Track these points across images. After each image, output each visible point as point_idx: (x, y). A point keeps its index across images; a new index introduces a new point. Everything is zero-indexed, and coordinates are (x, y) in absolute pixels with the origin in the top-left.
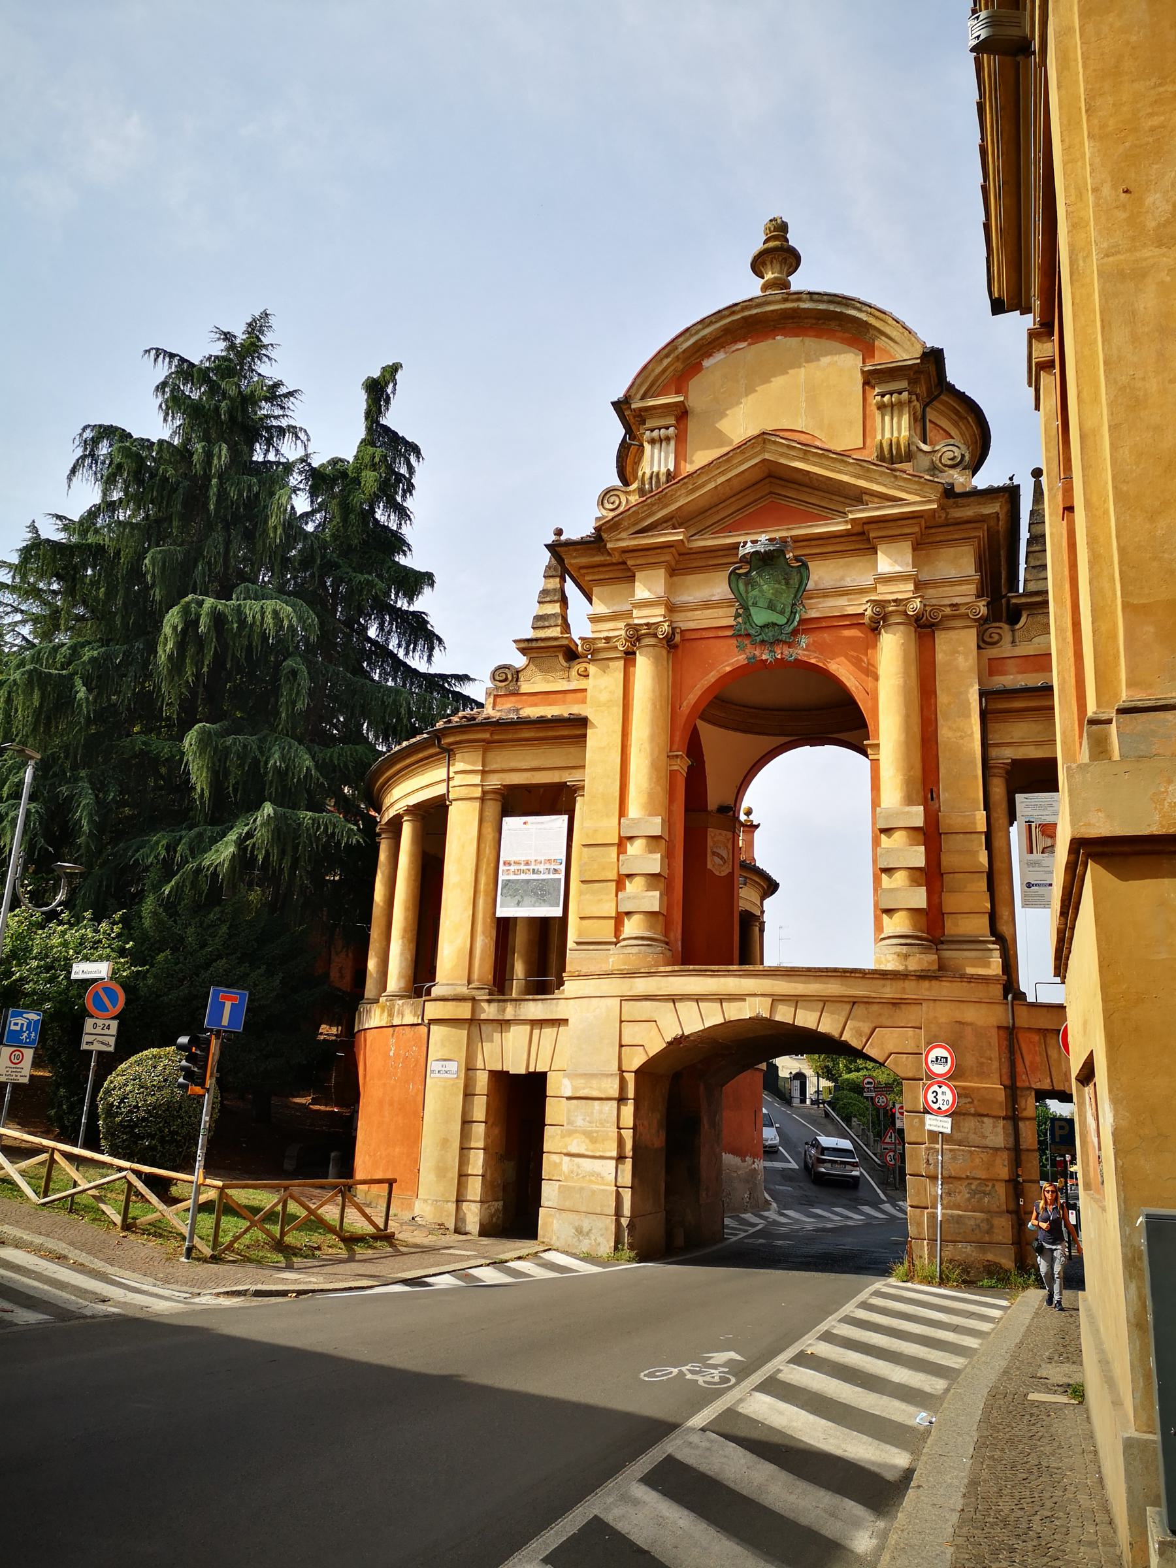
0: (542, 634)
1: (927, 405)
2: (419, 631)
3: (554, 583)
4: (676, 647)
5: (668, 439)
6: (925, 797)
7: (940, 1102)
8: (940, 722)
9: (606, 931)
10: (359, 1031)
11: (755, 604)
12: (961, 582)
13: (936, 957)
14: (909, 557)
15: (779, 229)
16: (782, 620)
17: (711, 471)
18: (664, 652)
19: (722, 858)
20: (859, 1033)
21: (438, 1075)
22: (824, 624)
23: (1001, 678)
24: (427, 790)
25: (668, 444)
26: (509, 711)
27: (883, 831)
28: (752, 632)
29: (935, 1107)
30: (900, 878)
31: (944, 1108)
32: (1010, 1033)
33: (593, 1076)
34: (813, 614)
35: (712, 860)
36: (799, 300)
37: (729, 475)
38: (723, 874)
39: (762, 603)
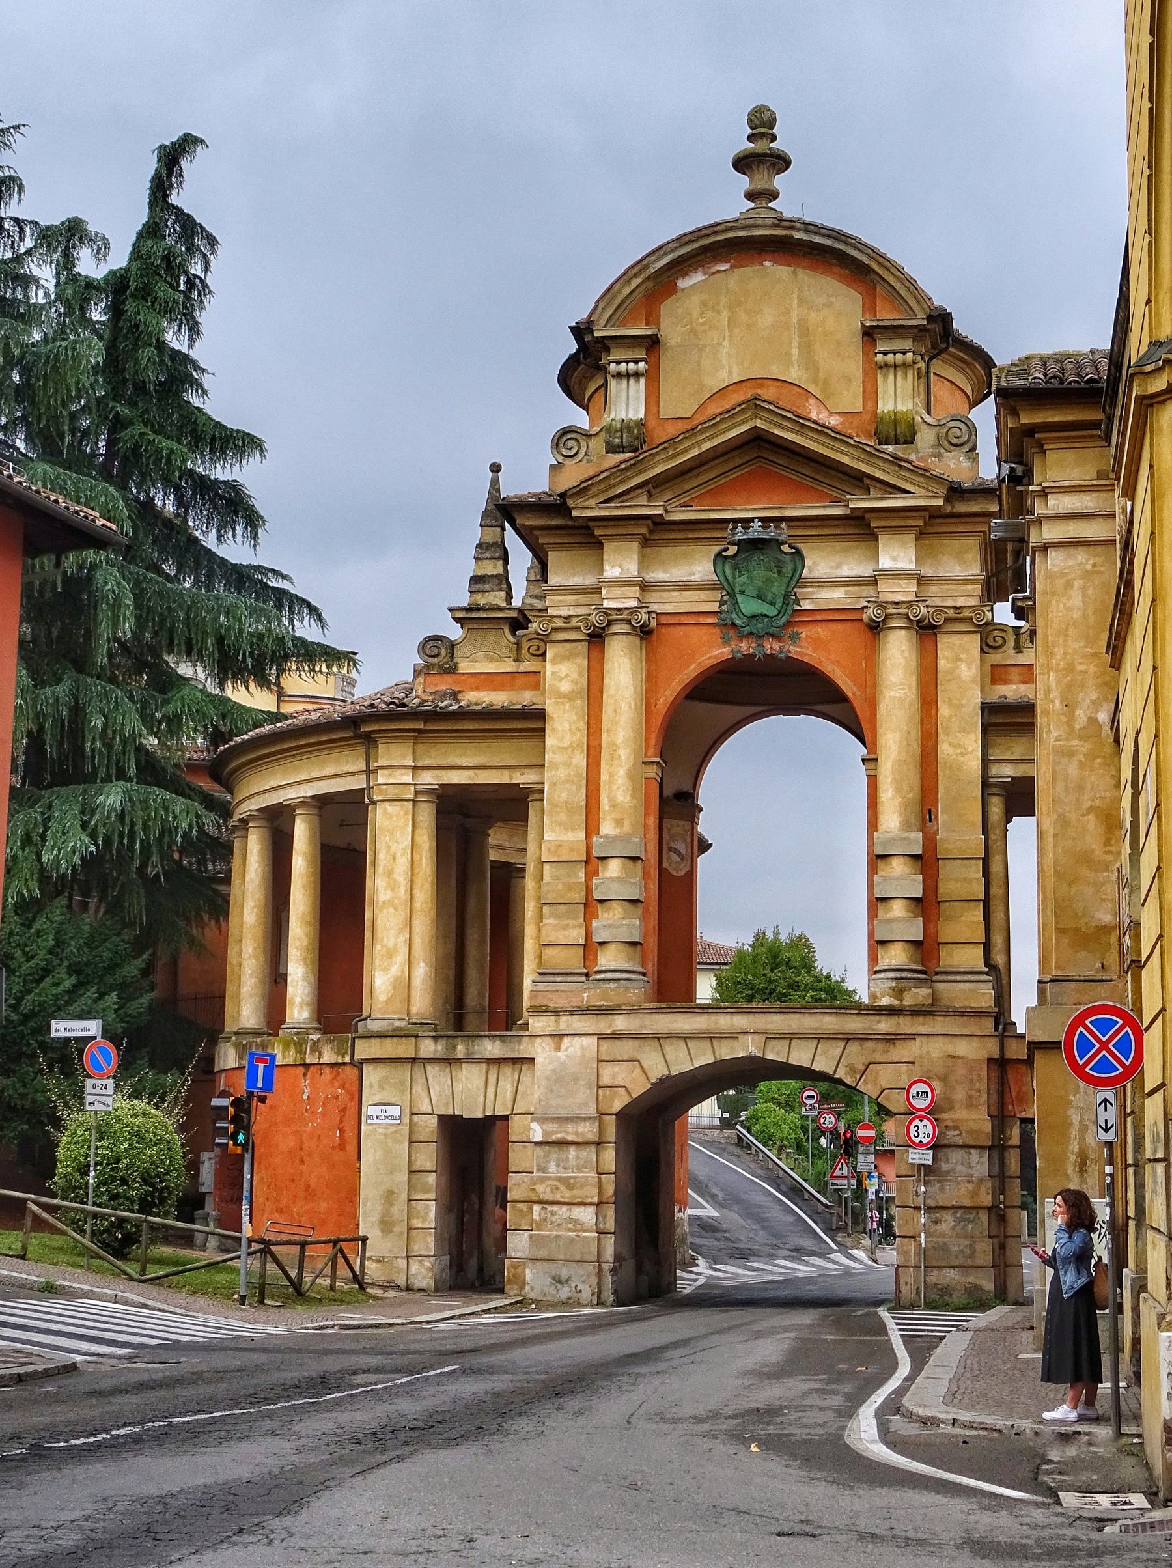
0: (482, 600)
1: (931, 358)
2: (234, 507)
3: (492, 535)
4: (650, 632)
5: (637, 375)
6: (924, 819)
7: (922, 1135)
8: (941, 736)
9: (573, 960)
10: (221, 1071)
11: (742, 592)
12: (966, 581)
13: (930, 991)
14: (912, 553)
15: (762, 123)
16: (772, 611)
17: (694, 435)
18: (638, 640)
19: (679, 854)
20: (852, 1069)
21: (376, 1121)
22: (818, 618)
23: (1003, 687)
24: (332, 781)
25: (638, 381)
26: (444, 695)
27: (878, 857)
28: (738, 622)
29: (917, 1140)
30: (898, 909)
31: (925, 1141)
32: (1000, 1065)
33: (567, 1119)
34: (806, 605)
35: (669, 857)
36: (792, 228)
37: (715, 442)
38: (681, 874)
39: (751, 591)
